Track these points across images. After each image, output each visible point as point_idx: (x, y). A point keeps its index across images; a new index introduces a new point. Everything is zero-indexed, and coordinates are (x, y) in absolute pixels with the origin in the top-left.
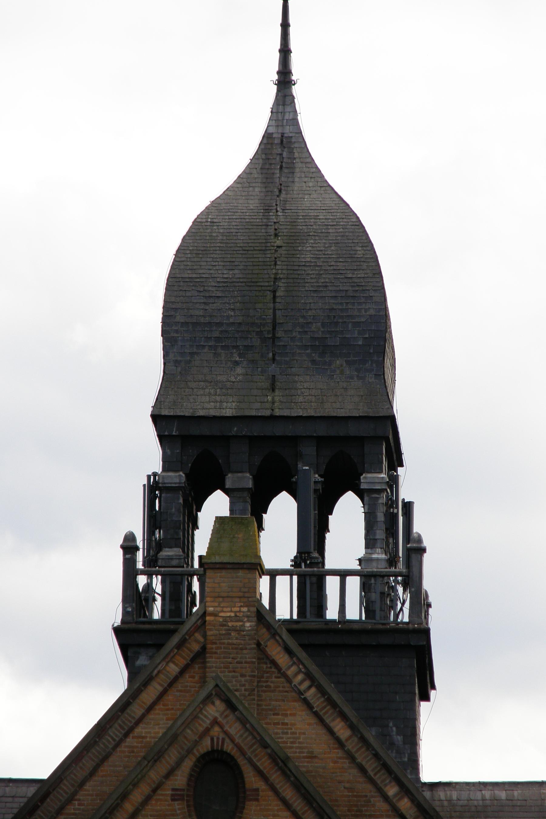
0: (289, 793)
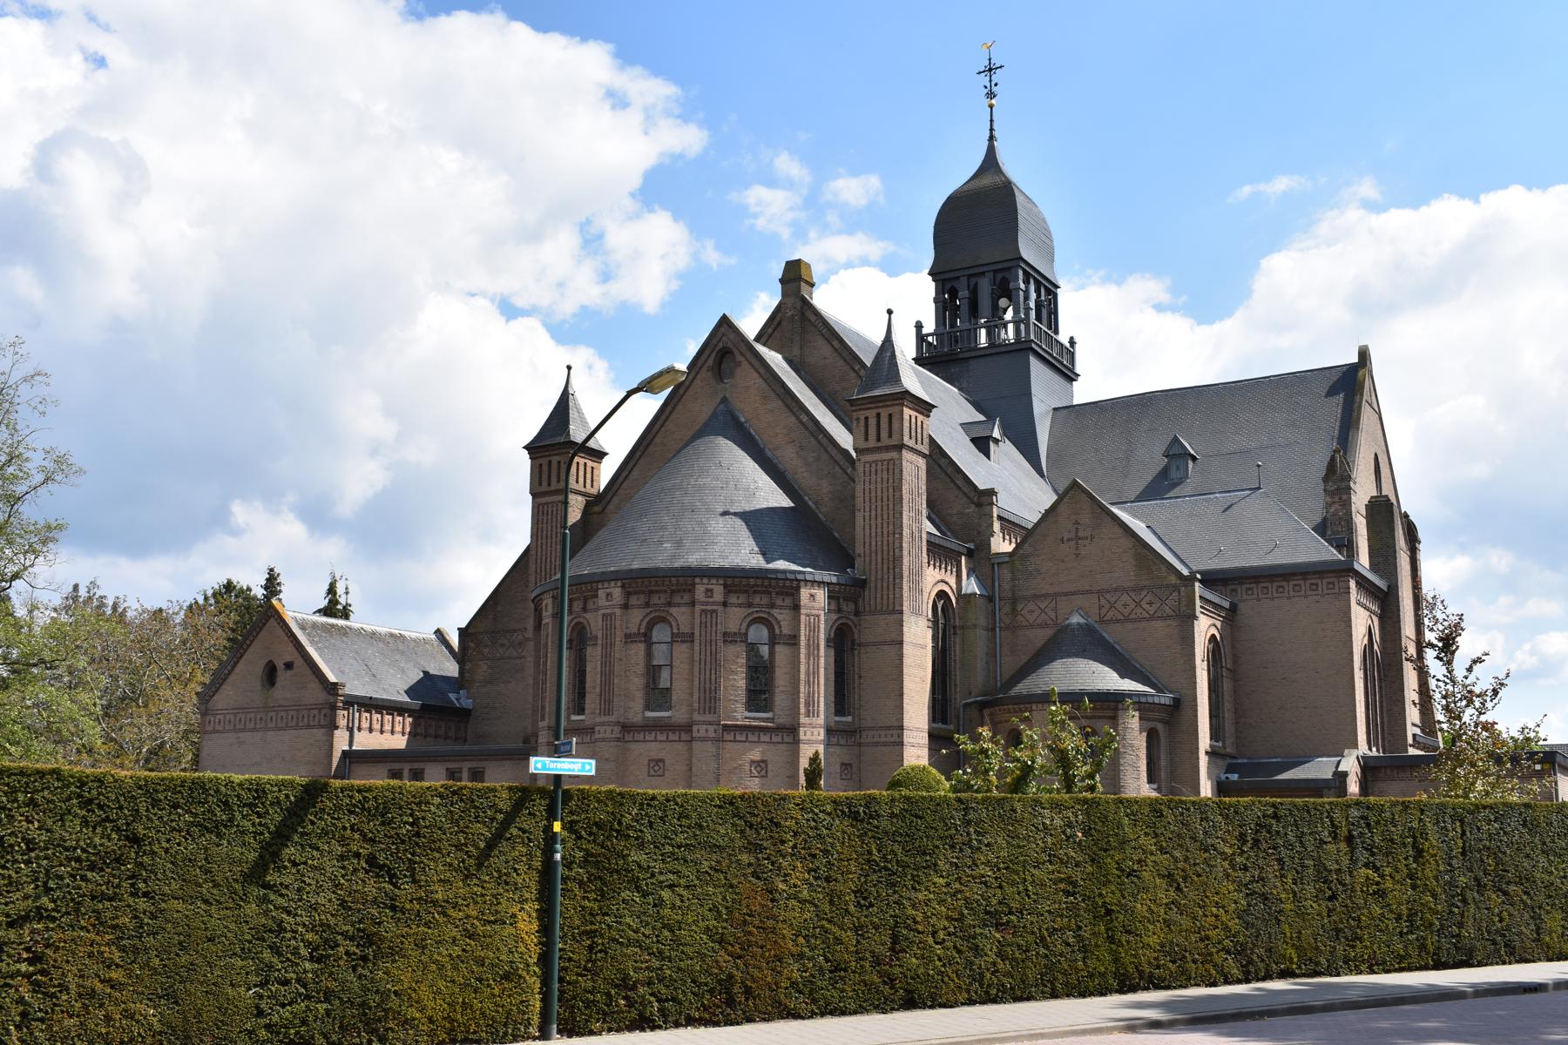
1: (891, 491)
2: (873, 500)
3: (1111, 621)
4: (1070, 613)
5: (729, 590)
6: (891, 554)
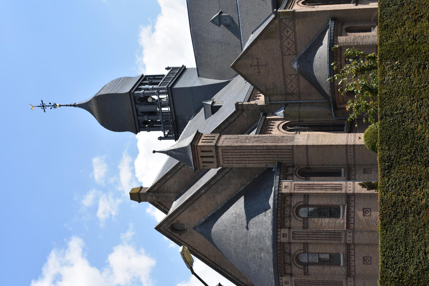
1: (236, 151)
2: (240, 159)
3: (296, 50)
4: (293, 68)
5: (283, 226)
6: (266, 151)
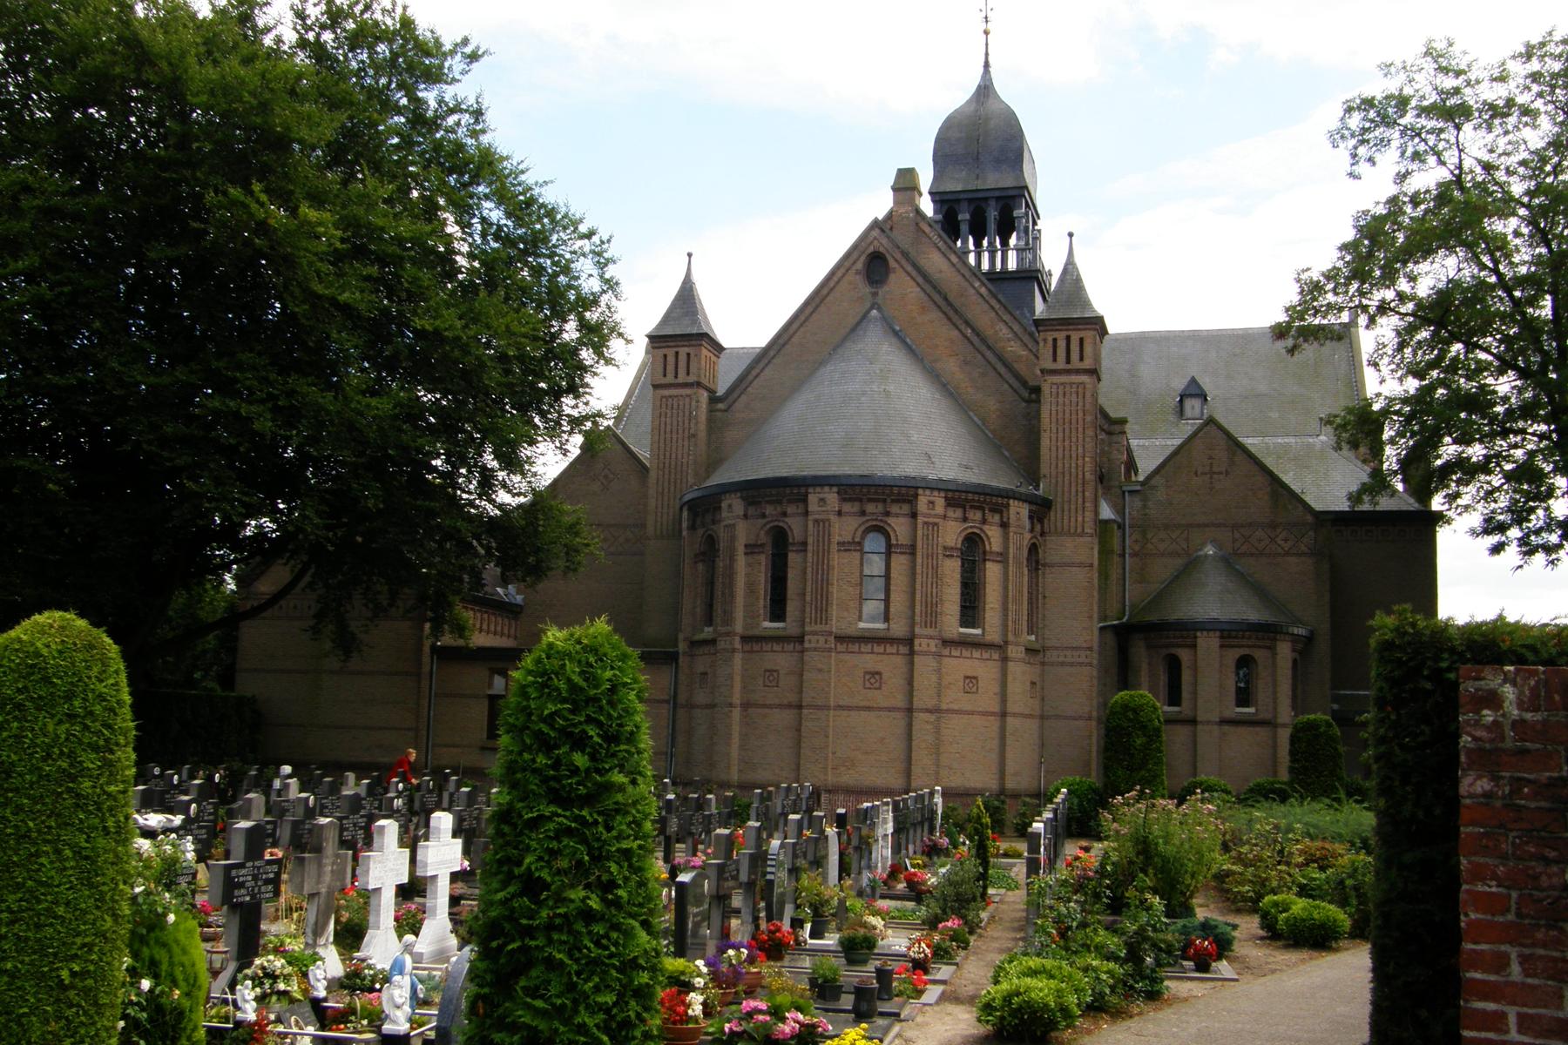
0: (909, 268)
1: (1081, 414)
2: (1061, 421)
3: (1244, 554)
4: (1204, 544)
5: (950, 503)
6: (1080, 476)
